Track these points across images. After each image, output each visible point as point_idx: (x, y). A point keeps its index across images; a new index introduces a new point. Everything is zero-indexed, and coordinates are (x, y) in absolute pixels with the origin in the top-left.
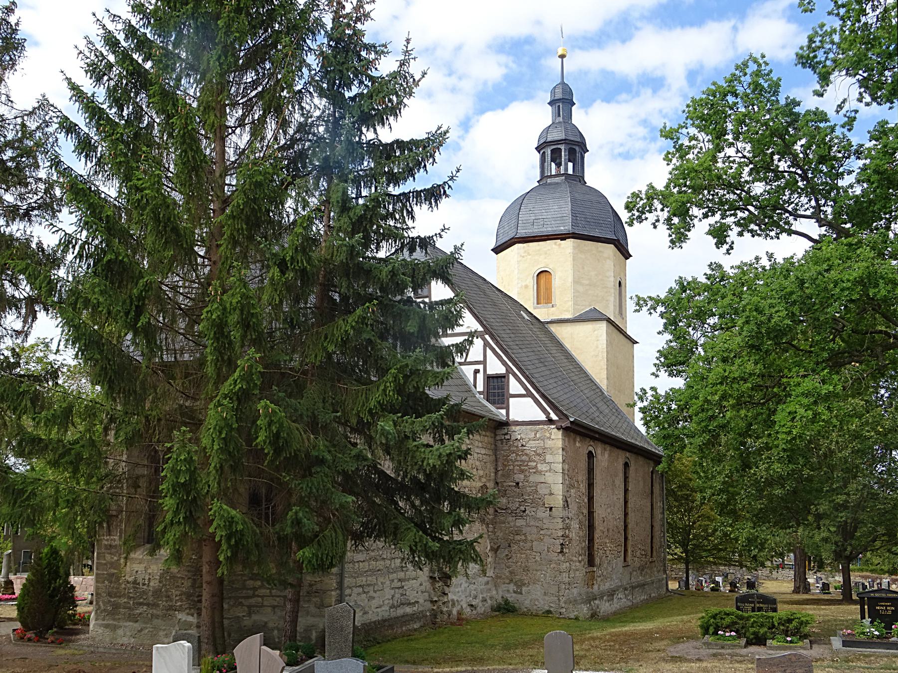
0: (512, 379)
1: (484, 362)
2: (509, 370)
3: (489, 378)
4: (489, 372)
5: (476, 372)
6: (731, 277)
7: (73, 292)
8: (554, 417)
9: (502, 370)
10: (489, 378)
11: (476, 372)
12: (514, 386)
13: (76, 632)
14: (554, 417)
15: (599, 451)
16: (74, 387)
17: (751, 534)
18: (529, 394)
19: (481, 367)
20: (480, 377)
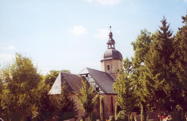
0: (99, 88)
1: (96, 86)
2: (99, 87)
3: (96, 88)
4: (96, 87)
5: (95, 87)
6: (61, 94)
7: (172, 92)
8: (105, 93)
9: (98, 87)
10: (96, 88)
11: (95, 87)
12: (100, 89)
13: (95, 113)
14: (105, 93)
15: (113, 96)
16: (182, 91)
17: (133, 75)
18: (102, 90)
19: (95, 87)
20: (95, 88)
